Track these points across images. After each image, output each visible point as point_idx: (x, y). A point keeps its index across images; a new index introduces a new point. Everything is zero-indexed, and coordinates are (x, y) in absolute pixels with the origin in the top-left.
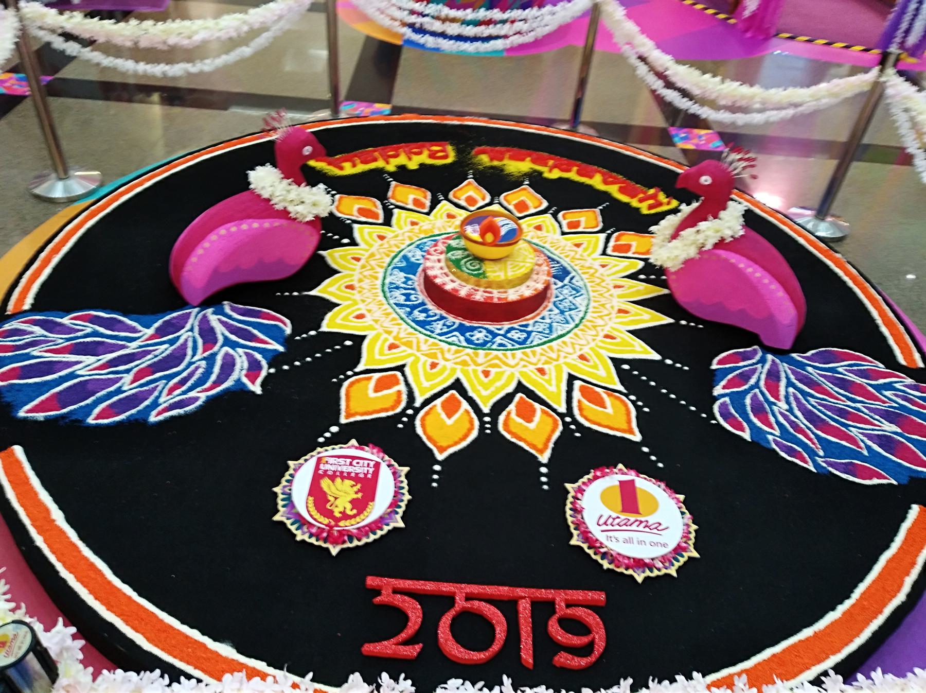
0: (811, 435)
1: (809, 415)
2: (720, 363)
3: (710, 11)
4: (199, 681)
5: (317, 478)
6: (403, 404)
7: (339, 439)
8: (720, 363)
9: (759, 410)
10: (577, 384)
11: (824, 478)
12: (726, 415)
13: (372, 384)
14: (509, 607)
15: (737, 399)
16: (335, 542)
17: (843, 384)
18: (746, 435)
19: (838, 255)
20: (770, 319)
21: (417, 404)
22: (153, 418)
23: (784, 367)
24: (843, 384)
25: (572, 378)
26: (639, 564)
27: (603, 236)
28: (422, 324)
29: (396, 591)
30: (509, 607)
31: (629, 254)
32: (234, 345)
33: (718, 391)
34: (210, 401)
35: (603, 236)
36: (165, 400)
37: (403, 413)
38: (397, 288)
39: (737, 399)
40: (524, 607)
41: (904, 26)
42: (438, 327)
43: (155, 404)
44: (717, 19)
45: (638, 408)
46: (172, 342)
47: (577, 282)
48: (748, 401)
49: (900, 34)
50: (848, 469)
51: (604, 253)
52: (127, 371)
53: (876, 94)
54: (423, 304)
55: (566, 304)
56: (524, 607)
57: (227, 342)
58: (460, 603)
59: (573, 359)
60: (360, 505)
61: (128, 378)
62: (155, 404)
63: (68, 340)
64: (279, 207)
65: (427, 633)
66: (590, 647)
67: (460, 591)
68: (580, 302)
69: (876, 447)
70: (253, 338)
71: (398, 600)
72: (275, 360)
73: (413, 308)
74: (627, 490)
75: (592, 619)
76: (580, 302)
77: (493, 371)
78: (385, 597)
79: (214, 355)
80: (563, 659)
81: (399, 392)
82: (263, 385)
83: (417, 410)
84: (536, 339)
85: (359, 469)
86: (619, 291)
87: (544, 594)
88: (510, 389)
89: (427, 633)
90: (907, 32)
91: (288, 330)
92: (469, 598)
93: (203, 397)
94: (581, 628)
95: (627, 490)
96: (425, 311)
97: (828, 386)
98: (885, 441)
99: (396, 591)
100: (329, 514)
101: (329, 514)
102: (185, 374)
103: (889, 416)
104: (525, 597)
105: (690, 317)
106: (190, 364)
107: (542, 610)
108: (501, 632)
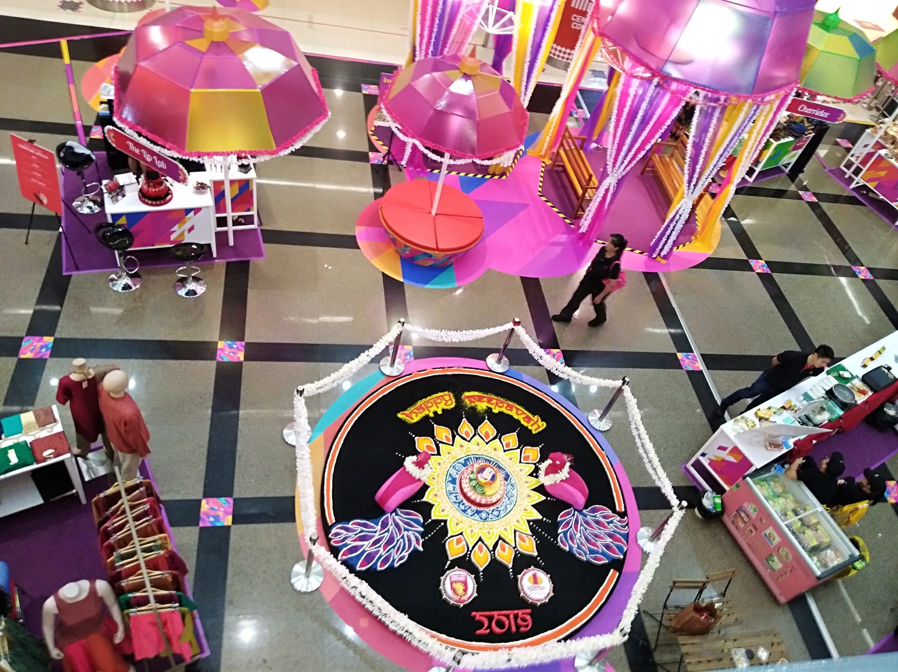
0: (586, 547)
1: (586, 539)
2: (561, 517)
3: (562, 215)
4: (478, 654)
5: (451, 583)
6: (466, 550)
7: (451, 567)
8: (561, 517)
9: (572, 538)
10: (517, 533)
11: (588, 563)
12: (562, 542)
13: (455, 542)
14: (508, 616)
15: (565, 533)
16: (462, 603)
17: (598, 522)
18: (567, 549)
19: (604, 452)
20: (577, 503)
21: (470, 549)
22: (396, 565)
23: (580, 517)
24: (598, 522)
25: (515, 532)
26: (538, 600)
27: (519, 450)
28: (464, 511)
29: (480, 616)
30: (508, 616)
31: (529, 462)
32: (408, 530)
33: (560, 531)
34: (410, 555)
35: (519, 450)
36: (397, 557)
37: (466, 554)
38: (452, 493)
39: (565, 533)
40: (512, 617)
41: (660, 247)
42: (469, 511)
43: (393, 561)
44: (565, 222)
45: (536, 542)
46: (388, 531)
47: (513, 482)
48: (568, 534)
49: (658, 250)
50: (596, 559)
51: (520, 462)
52: (380, 546)
53: (620, 390)
54: (462, 501)
55: (510, 494)
56: (512, 617)
57: (405, 530)
58: (496, 617)
59: (515, 522)
60: (465, 590)
61: (381, 549)
62: (393, 561)
63: (356, 535)
64: (417, 478)
65: (489, 627)
66: (527, 626)
67: (495, 613)
68: (514, 492)
69: (604, 549)
70: (412, 526)
71: (481, 618)
72: (423, 535)
73: (459, 503)
74: (535, 576)
75: (528, 617)
76: (514, 492)
77: (491, 531)
78: (478, 618)
79: (403, 536)
80: (522, 629)
81: (464, 545)
82: (423, 547)
83: (471, 551)
84: (502, 514)
85: (462, 579)
86: (527, 485)
87: (516, 612)
88: (497, 539)
89: (489, 627)
90: (661, 250)
91: (422, 521)
92: (498, 615)
93: (407, 554)
94: (524, 620)
95: (535, 576)
96: (463, 504)
97: (593, 524)
98: (607, 547)
99: (480, 616)
100: (457, 595)
101: (457, 595)
102: (398, 545)
103: (610, 536)
104: (511, 613)
105: (551, 497)
106: (398, 541)
107: (516, 617)
108: (507, 623)
